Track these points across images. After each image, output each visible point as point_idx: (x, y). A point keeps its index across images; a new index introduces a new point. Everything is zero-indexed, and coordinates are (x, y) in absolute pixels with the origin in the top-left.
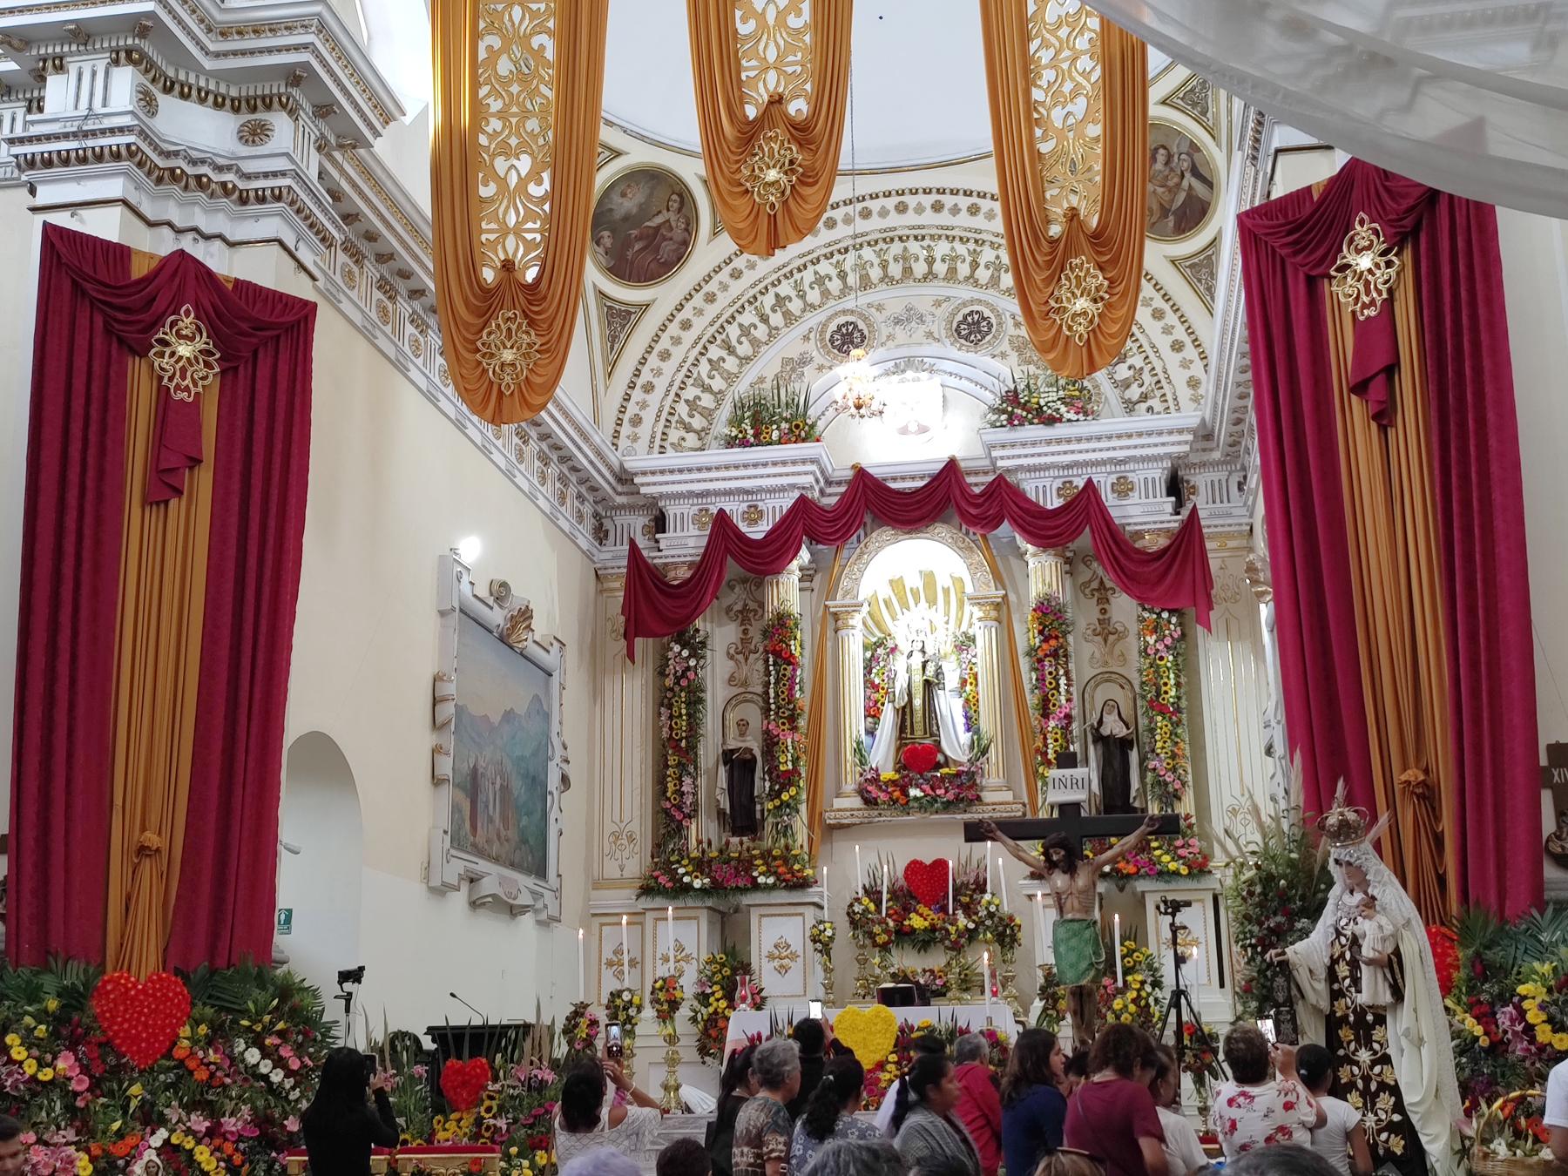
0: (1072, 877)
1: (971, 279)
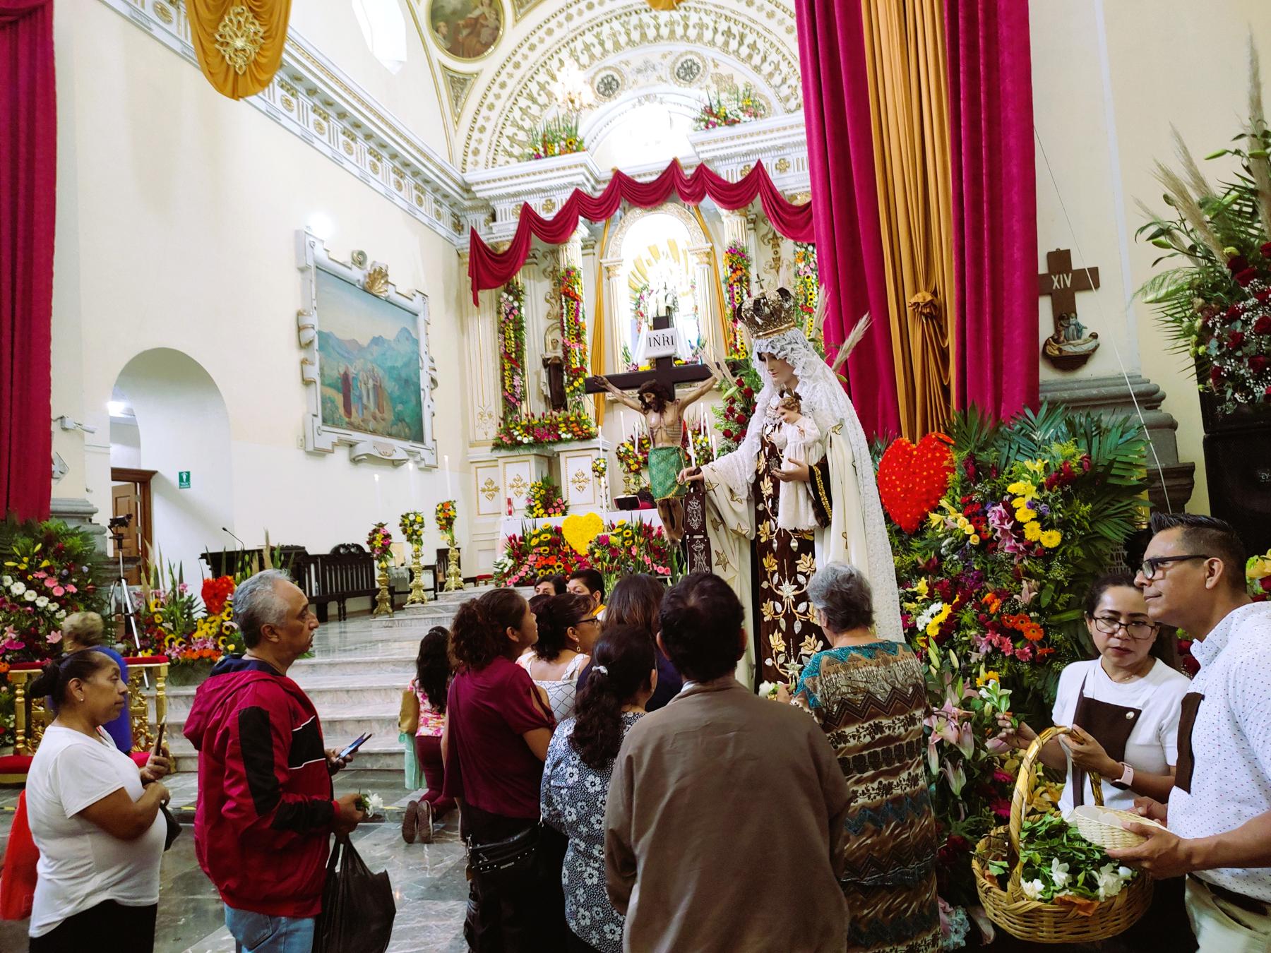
0: (661, 414)
1: (685, 37)
